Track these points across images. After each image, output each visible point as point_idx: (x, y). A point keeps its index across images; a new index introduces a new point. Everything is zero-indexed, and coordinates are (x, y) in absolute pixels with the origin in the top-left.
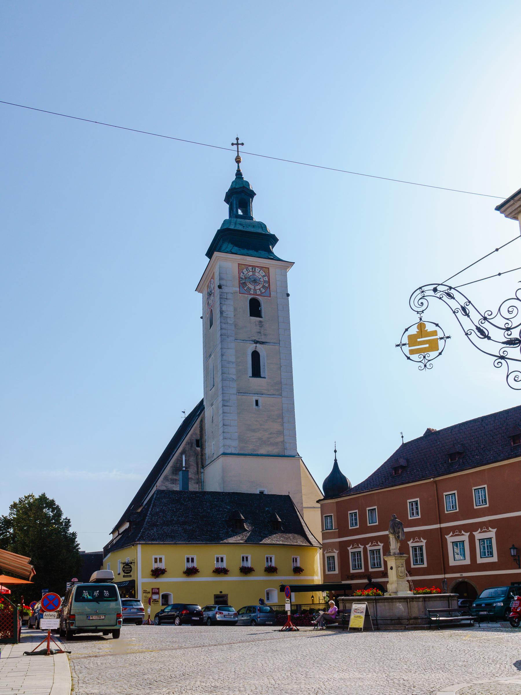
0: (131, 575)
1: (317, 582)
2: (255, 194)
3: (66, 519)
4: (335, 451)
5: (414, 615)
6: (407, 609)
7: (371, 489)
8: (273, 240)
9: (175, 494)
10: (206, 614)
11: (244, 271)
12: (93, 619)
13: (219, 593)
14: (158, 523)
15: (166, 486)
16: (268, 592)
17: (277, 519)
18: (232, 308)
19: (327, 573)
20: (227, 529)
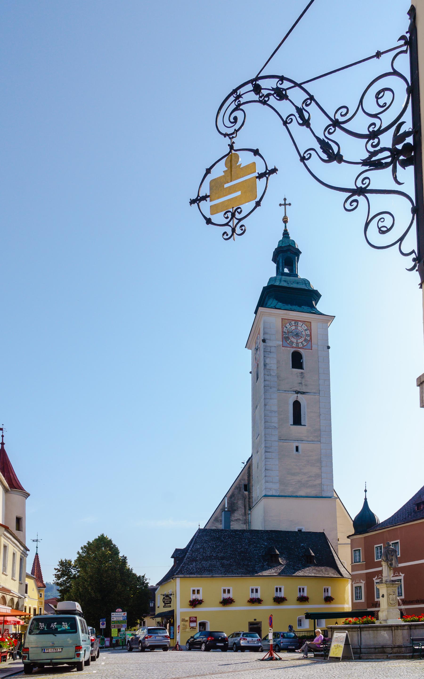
1: (346, 610)
3: (123, 557)
4: (366, 491)
5: (398, 644)
6: (391, 637)
7: (395, 524)
10: (231, 641)
11: (287, 325)
12: (49, 652)
13: (253, 621)
14: (197, 558)
15: (216, 527)
16: (300, 619)
17: (311, 553)
18: (275, 361)
19: (355, 601)
20: (263, 563)
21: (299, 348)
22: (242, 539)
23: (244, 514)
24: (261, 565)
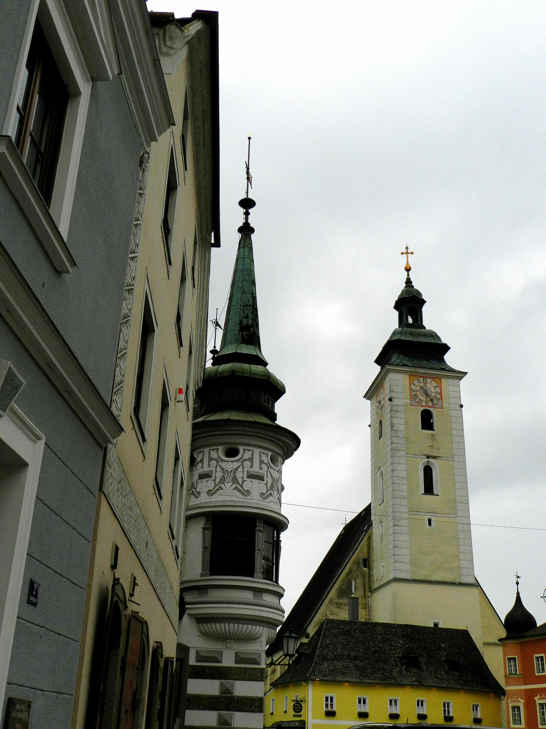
0: (301, 715)
2: (425, 302)
8: (445, 348)
9: (345, 624)
11: (415, 382)
14: (329, 657)
18: (402, 421)
20: (400, 668)
21: (429, 407)
22: (374, 635)
23: (363, 596)
24: (399, 670)
